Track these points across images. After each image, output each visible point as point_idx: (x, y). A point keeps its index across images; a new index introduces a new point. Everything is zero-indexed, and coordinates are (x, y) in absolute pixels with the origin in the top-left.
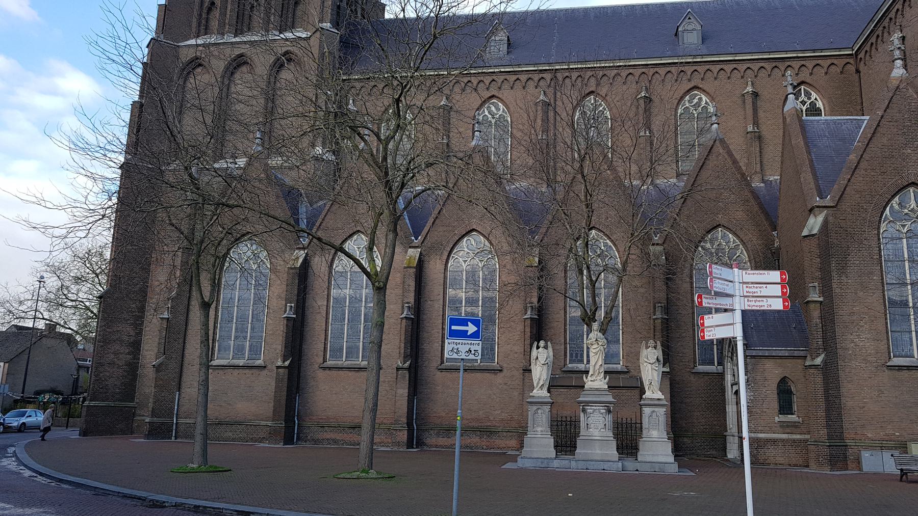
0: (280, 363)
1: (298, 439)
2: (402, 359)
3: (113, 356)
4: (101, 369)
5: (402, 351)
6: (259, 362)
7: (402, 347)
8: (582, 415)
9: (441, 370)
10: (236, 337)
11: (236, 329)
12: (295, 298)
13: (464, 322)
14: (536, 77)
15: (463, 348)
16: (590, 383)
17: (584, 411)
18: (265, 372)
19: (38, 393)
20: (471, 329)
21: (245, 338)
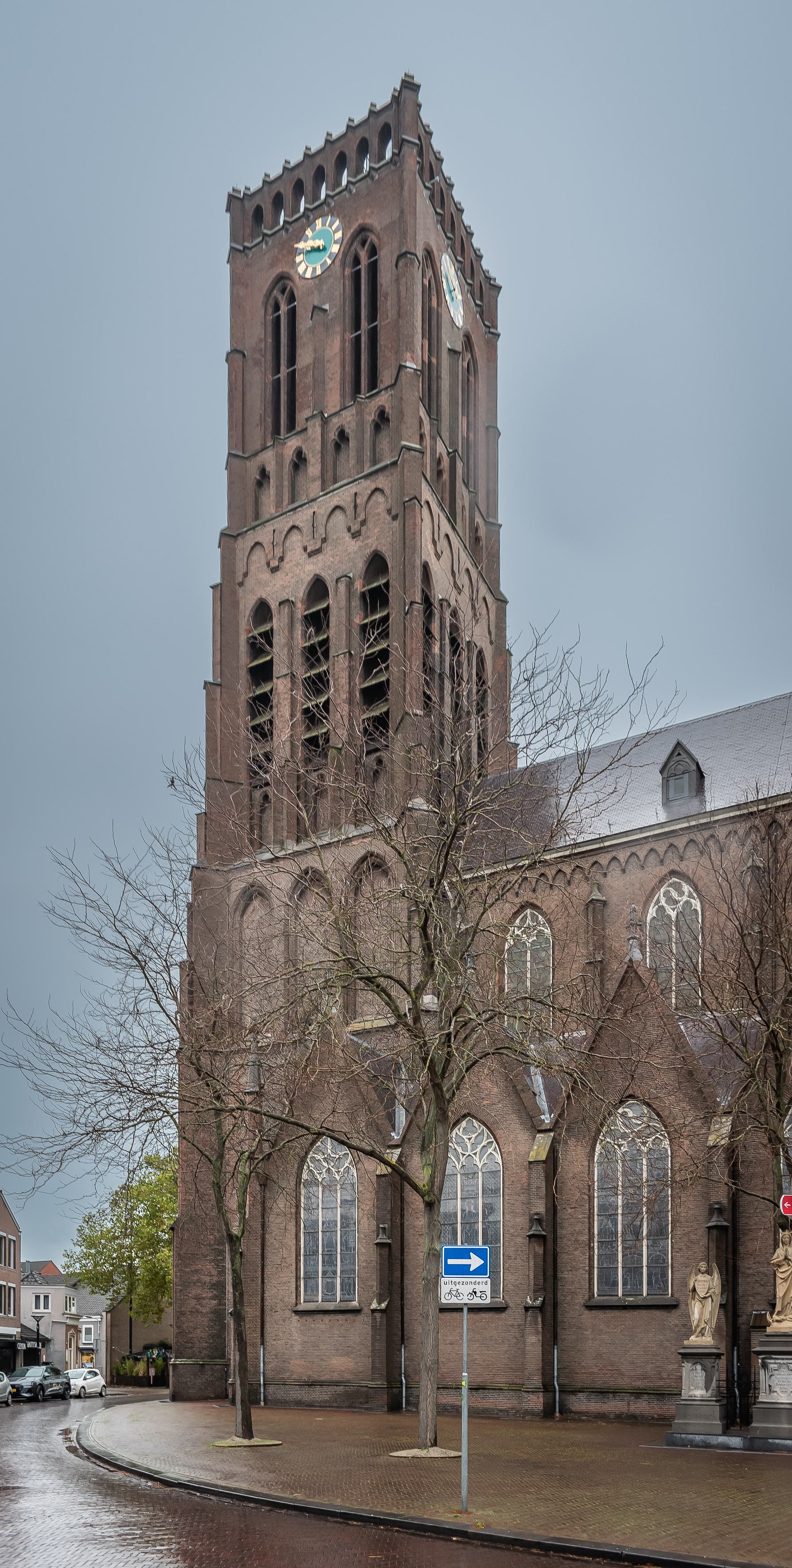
0: (374, 1305)
1: (408, 1403)
2: (531, 1293)
3: (194, 1302)
4: (183, 1319)
5: (532, 1283)
6: (355, 1304)
7: (532, 1277)
8: (762, 1372)
9: (590, 1308)
10: (324, 1273)
11: (323, 1262)
12: (389, 1217)
13: (465, 1254)
14: (699, 838)
15: (466, 1290)
16: (775, 1325)
17: (765, 1366)
18: (360, 1318)
19: (148, 1347)
20: (475, 1262)
21: (335, 1273)
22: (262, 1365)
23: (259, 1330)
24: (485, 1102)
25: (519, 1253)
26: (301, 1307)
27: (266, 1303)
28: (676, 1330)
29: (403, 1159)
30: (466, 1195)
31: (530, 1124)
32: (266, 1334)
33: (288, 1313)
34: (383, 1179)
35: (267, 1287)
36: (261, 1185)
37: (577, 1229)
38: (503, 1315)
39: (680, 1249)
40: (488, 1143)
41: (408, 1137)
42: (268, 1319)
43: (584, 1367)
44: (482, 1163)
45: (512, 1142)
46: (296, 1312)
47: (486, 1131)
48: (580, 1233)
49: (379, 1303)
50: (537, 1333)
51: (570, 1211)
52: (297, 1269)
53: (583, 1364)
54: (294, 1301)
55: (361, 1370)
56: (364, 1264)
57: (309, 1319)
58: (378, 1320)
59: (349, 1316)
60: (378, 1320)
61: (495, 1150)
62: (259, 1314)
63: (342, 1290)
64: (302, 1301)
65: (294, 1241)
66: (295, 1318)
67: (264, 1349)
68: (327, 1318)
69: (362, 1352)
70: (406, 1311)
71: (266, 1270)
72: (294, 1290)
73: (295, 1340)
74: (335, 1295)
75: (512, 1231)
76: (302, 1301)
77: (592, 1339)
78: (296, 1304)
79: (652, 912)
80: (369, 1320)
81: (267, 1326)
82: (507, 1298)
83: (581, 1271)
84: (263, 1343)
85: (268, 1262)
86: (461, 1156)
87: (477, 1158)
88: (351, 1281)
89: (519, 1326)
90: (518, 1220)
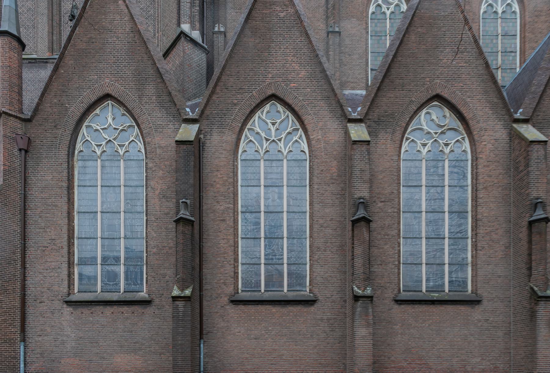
0: (176, 292)
6: (143, 295)
22: (22, 366)
23: (18, 324)
24: (292, 85)
25: (329, 244)
26: (73, 298)
27: (28, 292)
28: (479, 324)
29: (202, 136)
30: (269, 183)
31: (340, 112)
32: (28, 329)
33: (58, 304)
34: (185, 147)
35: (30, 273)
36: (20, 150)
37: (387, 223)
38: (312, 309)
39: (483, 248)
40: (294, 130)
41: (207, 112)
42: (30, 310)
43: (393, 361)
44: (287, 151)
45: (321, 129)
46: (69, 303)
47: (291, 117)
48: (389, 227)
49: (182, 290)
50: (368, 325)
51: (380, 204)
52: (69, 253)
53: (393, 358)
54: (66, 290)
55: (151, 368)
56: (155, 250)
57: (86, 311)
58: (181, 309)
59: (137, 309)
60: (181, 309)
61: (300, 137)
62: (18, 304)
63: (126, 279)
64: (76, 291)
65: (66, 221)
66: (67, 310)
67: (25, 347)
68: (108, 310)
69: (152, 349)
70: (205, 303)
71: (28, 253)
72: (66, 277)
73: (68, 336)
74: (118, 284)
75: (321, 221)
76: (76, 291)
77: (402, 334)
78: (69, 294)
79: (372, 9)
80: (168, 309)
81: (30, 319)
82: (316, 291)
83: (390, 265)
84: (24, 340)
85: (30, 243)
86: (264, 141)
87: (281, 144)
88: (138, 269)
89: (328, 320)
90: (327, 211)
